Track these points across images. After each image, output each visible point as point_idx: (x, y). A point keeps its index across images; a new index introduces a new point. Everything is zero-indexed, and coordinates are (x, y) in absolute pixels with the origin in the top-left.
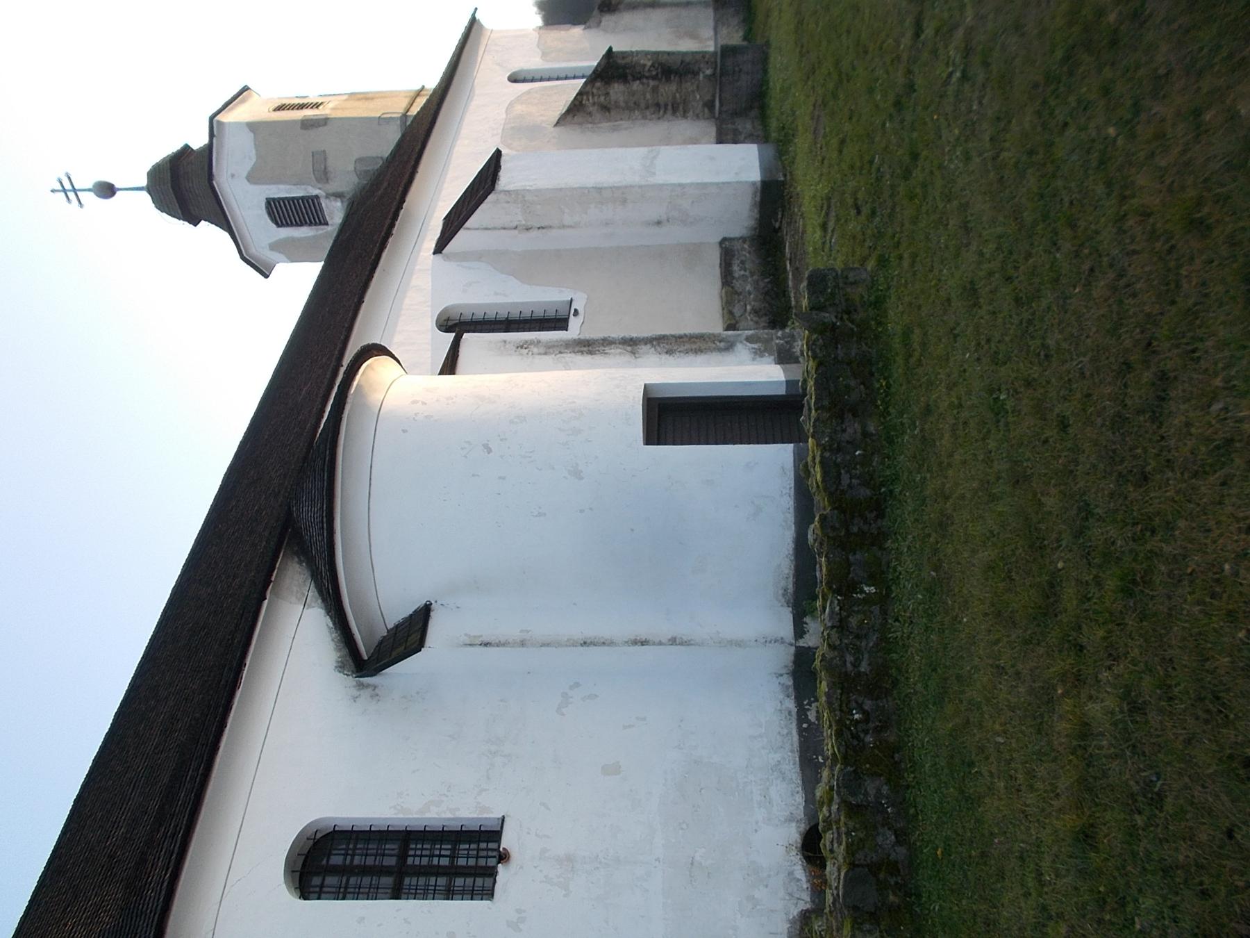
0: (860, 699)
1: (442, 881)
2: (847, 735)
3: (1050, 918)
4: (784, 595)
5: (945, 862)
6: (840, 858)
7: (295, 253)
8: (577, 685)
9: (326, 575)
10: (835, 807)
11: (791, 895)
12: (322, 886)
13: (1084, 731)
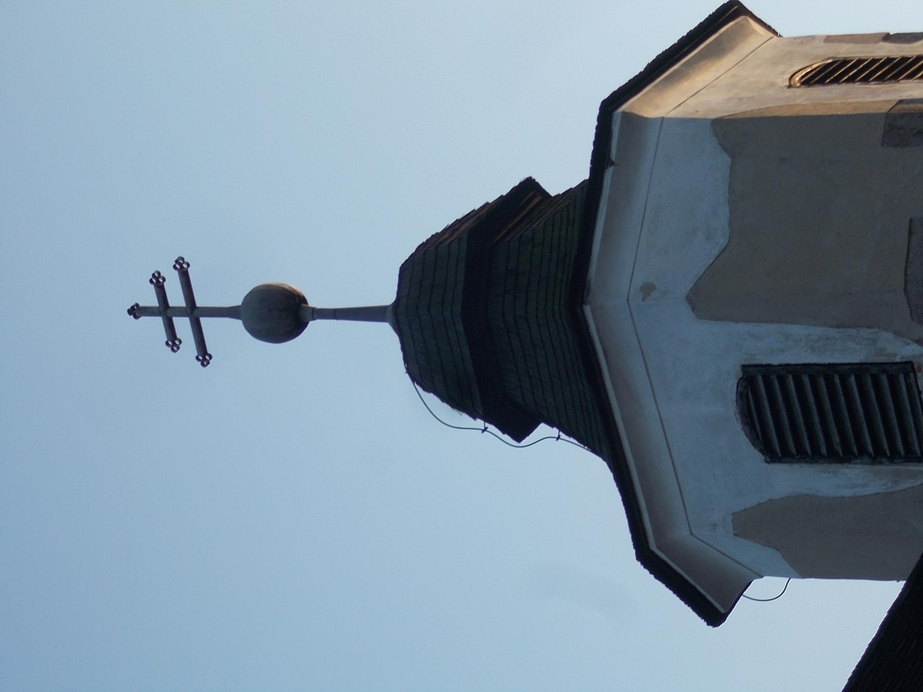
7: (818, 548)
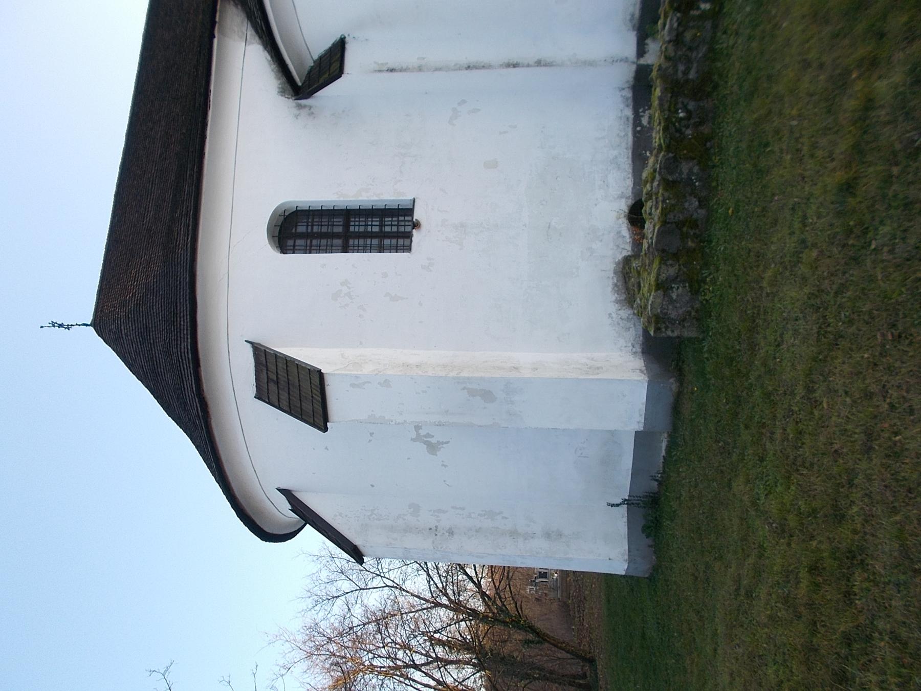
0: (686, 101)
1: (375, 242)
2: (672, 130)
3: (806, 247)
4: (631, 20)
5: (734, 217)
6: (656, 218)
8: (464, 102)
9: (257, 14)
10: (656, 184)
11: (618, 246)
12: (294, 246)
13: (869, 104)
